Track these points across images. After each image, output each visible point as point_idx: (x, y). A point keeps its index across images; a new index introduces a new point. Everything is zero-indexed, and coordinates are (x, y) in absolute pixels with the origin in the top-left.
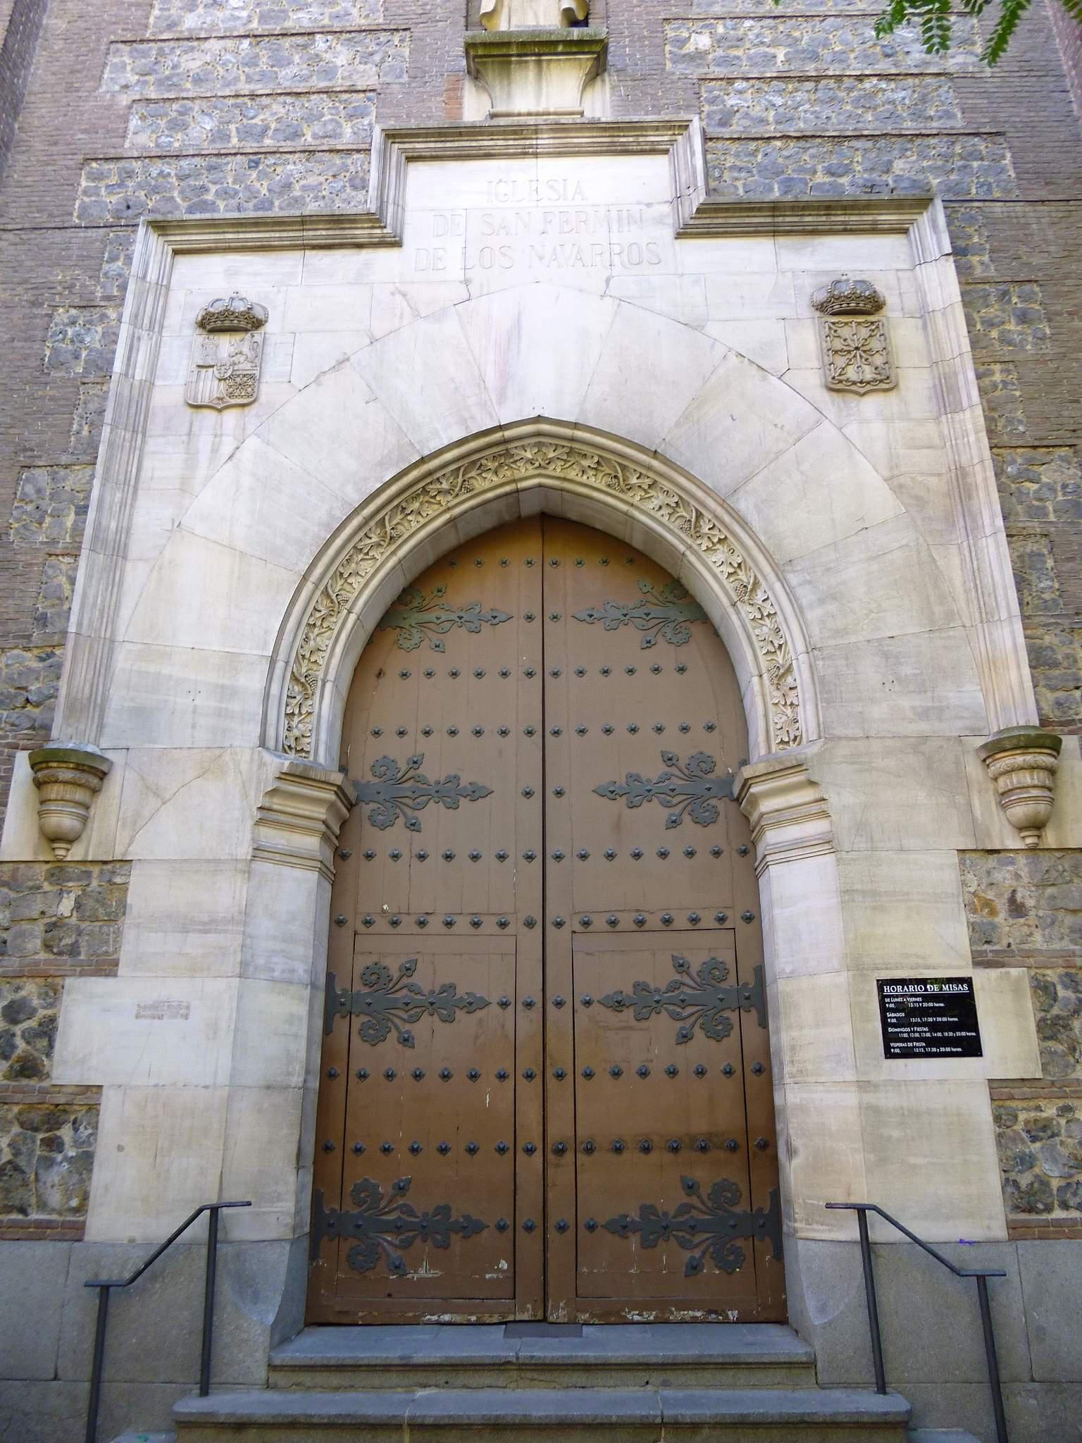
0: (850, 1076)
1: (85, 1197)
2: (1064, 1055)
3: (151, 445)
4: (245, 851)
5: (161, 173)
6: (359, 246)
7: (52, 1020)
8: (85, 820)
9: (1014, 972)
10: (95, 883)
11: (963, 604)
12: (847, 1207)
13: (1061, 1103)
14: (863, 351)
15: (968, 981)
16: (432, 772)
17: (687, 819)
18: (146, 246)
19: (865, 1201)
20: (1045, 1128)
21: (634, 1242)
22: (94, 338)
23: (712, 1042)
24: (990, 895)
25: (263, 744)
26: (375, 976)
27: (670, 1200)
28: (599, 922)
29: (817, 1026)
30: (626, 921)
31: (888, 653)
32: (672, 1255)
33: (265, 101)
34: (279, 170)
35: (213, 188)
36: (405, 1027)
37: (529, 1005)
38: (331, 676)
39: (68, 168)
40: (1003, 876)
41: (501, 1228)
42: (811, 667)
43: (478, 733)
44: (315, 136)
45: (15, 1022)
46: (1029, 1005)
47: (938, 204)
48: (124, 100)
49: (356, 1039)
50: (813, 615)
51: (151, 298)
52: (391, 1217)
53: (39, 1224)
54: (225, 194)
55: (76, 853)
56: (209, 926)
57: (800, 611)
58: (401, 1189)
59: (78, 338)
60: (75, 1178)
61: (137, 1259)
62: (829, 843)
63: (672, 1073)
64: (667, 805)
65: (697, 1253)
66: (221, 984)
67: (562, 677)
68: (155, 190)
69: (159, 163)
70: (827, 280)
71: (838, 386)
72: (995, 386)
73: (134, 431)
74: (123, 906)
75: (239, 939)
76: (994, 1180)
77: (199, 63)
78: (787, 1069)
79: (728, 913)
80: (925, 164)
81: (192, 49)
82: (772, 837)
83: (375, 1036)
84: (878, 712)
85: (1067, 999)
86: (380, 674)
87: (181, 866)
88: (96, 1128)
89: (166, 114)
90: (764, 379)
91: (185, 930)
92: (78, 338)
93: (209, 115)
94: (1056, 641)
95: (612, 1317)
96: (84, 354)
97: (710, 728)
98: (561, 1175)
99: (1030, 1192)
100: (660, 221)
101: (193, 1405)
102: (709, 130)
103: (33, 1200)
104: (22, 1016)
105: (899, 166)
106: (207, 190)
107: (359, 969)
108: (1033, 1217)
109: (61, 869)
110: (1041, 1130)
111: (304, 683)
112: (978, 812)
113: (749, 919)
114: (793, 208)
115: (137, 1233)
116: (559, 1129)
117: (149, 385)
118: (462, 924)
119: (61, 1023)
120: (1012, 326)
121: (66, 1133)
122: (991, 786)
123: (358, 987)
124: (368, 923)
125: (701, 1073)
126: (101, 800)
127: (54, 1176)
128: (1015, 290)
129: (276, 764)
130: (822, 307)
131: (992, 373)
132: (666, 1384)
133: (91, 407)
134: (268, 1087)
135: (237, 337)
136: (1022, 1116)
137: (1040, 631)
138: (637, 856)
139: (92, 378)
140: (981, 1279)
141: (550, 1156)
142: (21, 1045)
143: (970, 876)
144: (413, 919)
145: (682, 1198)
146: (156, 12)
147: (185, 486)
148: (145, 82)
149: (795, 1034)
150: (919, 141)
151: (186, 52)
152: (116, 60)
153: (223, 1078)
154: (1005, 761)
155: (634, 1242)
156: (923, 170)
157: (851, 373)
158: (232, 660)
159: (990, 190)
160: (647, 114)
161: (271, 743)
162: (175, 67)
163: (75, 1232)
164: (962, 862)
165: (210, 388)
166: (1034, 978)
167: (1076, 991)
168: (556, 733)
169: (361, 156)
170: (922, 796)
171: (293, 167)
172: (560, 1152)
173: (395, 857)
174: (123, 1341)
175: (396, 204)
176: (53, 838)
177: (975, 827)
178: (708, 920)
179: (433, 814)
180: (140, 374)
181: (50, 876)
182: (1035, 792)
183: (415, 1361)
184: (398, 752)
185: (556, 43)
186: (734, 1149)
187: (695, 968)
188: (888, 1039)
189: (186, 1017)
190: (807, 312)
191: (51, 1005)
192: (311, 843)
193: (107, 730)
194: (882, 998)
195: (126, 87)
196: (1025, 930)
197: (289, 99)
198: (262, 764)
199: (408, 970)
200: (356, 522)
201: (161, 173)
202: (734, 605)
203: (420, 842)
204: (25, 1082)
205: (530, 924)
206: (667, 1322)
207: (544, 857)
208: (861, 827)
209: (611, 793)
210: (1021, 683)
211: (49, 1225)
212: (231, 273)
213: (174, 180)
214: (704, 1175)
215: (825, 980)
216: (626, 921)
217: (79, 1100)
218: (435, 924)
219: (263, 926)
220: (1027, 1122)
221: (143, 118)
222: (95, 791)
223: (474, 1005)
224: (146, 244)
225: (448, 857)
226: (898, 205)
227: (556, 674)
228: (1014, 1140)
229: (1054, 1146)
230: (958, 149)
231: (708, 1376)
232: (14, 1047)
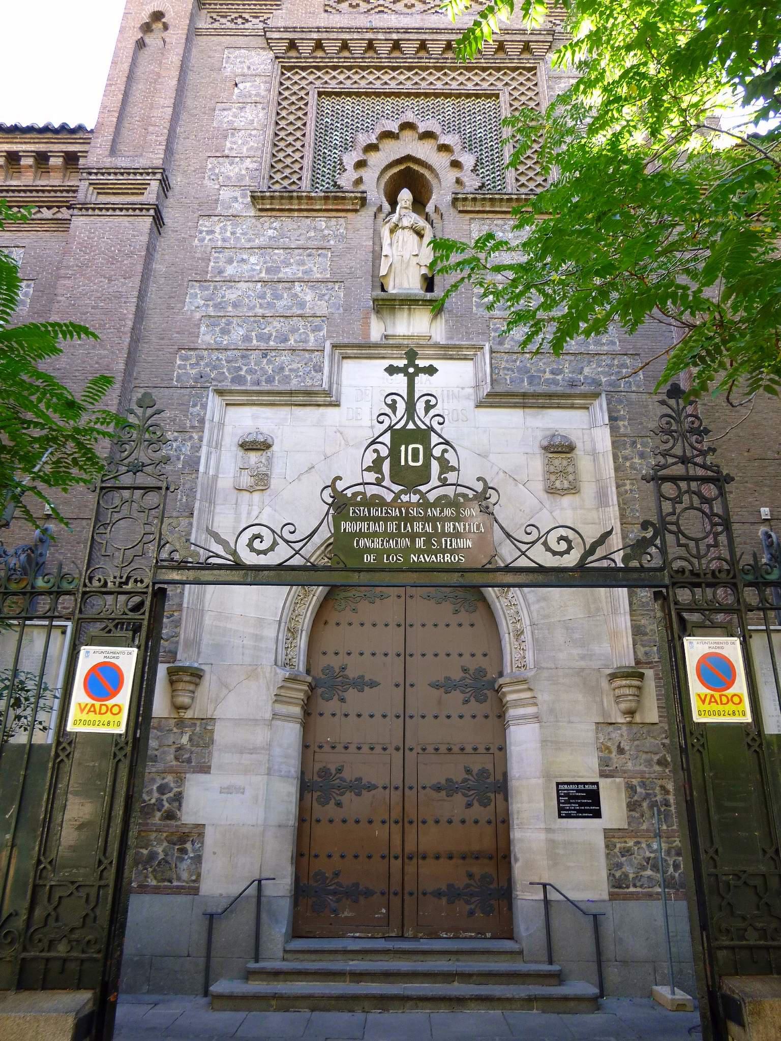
0: (543, 826)
1: (199, 875)
2: (638, 818)
3: (218, 509)
4: (268, 715)
5: (218, 358)
6: (319, 405)
7: (180, 793)
8: (193, 698)
9: (618, 780)
10: (198, 729)
11: (604, 604)
12: (538, 884)
13: (635, 840)
14: (563, 473)
15: (597, 784)
16: (352, 673)
17: (472, 699)
18: (214, 402)
19: (547, 882)
20: (628, 851)
21: (444, 900)
22: (187, 449)
23: (482, 808)
24: (609, 744)
25: (276, 664)
26: (324, 773)
27: (461, 882)
28: (430, 749)
29: (529, 802)
30: (443, 749)
31: (568, 626)
32: (461, 907)
33: (270, 320)
34: (277, 359)
35: (245, 368)
36: (338, 798)
37: (397, 788)
38: (305, 628)
39: (170, 353)
40: (616, 735)
41: (383, 894)
42: (532, 633)
43: (373, 654)
44: (295, 341)
45: (163, 794)
46: (624, 796)
47: (603, 396)
48: (198, 315)
49: (315, 804)
50: (534, 608)
51: (216, 431)
52: (332, 888)
53: (177, 887)
54: (250, 371)
55: (189, 714)
56: (253, 751)
57: (528, 606)
58: (337, 874)
59: (178, 449)
60: (194, 867)
61: (224, 903)
62: (537, 718)
63: (463, 822)
64: (463, 692)
65: (473, 906)
66: (259, 778)
67: (414, 627)
68: (215, 368)
69: (216, 353)
70: (548, 433)
71: (552, 491)
72: (626, 492)
73: (210, 502)
74: (212, 741)
75: (267, 757)
76: (604, 874)
77: (235, 296)
78: (515, 821)
79: (491, 746)
80: (600, 369)
81: (231, 287)
82: (512, 712)
83: (324, 802)
84: (562, 656)
85: (641, 793)
86: (326, 623)
87: (239, 722)
88: (202, 843)
89: (219, 325)
90: (516, 485)
91: (241, 753)
92: (178, 449)
93: (241, 326)
94: (647, 622)
95: (434, 935)
96: (182, 457)
97: (485, 655)
98: (411, 868)
99: (620, 879)
100: (468, 398)
101: (252, 965)
102: (494, 347)
103: (175, 876)
104: (166, 791)
105: (586, 371)
106: (241, 369)
107: (316, 769)
108: (621, 890)
109: (182, 722)
110: (627, 852)
111: (292, 632)
112: (605, 704)
113: (500, 749)
114: (533, 396)
115: (224, 893)
116: (410, 847)
117: (215, 477)
118: (365, 749)
119: (185, 795)
120: (636, 460)
121: (188, 846)
122: (612, 693)
123: (316, 778)
124: (321, 747)
125: (476, 822)
126: (200, 689)
127: (184, 865)
128: (639, 440)
129: (282, 674)
130: (545, 448)
131: (625, 485)
132: (458, 960)
133: (187, 486)
134: (279, 826)
135: (259, 453)
136: (618, 845)
137: (640, 617)
138: (449, 717)
139: (186, 471)
140: (595, 916)
141: (406, 860)
142: (166, 805)
143: (600, 735)
144: (342, 745)
145: (467, 881)
146: (212, 264)
148: (208, 305)
149: (519, 805)
150: (597, 357)
151: (228, 289)
152: (192, 291)
153: (260, 822)
154: (619, 682)
155: (444, 900)
156: (598, 373)
157: (558, 484)
158: (260, 622)
159: (630, 387)
160: (462, 339)
161: (279, 663)
162: (223, 297)
163: (195, 891)
164: (597, 728)
165: (246, 480)
166: (627, 783)
167: (646, 789)
168: (411, 655)
169: (319, 353)
170: (580, 697)
171: (285, 358)
172: (410, 858)
173: (334, 715)
174: (220, 939)
175: (338, 384)
176: (178, 708)
177: (604, 713)
178: (482, 749)
179: (351, 694)
180: (212, 472)
181: (177, 725)
182: (630, 698)
183: (349, 949)
184: (335, 663)
185: (419, 300)
186: (491, 858)
187: (475, 771)
188: (560, 809)
189: (243, 793)
190: (538, 451)
191: (179, 787)
192: (297, 710)
193: (202, 655)
194: (558, 790)
195: (198, 307)
196: (624, 761)
197: (282, 319)
198: (276, 674)
199: (339, 770)
200: (318, 553)
201: (218, 358)
202: (498, 598)
203: (345, 708)
204: (169, 822)
205: (397, 749)
206: (458, 938)
207: (404, 716)
208: (552, 711)
209: (436, 686)
210: (628, 647)
211: (182, 887)
212: (255, 417)
213: (224, 362)
214: (476, 870)
215: (534, 781)
216: (443, 749)
217: (195, 830)
218: (353, 748)
219: (277, 751)
220: (620, 848)
221: (207, 326)
222: (197, 685)
223: (371, 787)
224: (213, 402)
225: (359, 716)
226: (584, 396)
227: (411, 626)
228: (614, 856)
229: (631, 860)
230: (616, 362)
231: (476, 957)
232: (163, 806)
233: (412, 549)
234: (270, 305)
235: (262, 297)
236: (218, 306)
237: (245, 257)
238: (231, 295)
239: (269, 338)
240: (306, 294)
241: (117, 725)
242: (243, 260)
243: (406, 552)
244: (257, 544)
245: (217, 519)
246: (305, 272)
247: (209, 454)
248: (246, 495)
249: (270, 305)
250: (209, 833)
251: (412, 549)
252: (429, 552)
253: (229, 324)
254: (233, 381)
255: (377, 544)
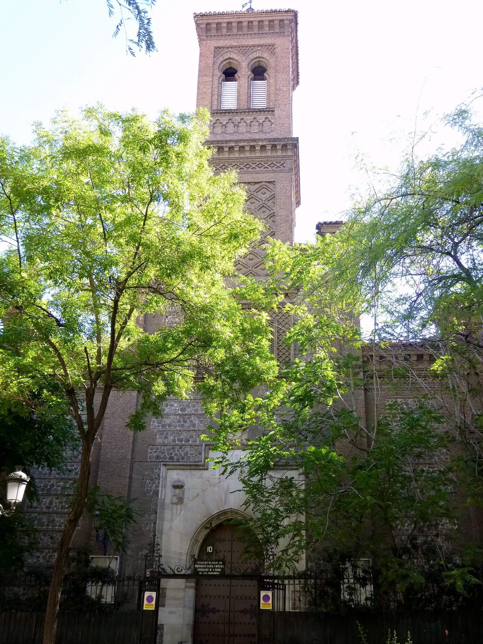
1: (162, 641)
4: (184, 587)
18: (163, 469)
26: (203, 606)
28: (239, 598)
30: (243, 597)
48: (155, 431)
56: (179, 599)
59: (151, 487)
68: (163, 453)
74: (165, 596)
111: (196, 541)
117: (164, 499)
118: (217, 597)
147: (172, 520)
158: (181, 554)
165: (175, 500)
199: (208, 605)
205: (228, 597)
216: (243, 597)
219: (187, 599)
223: (219, 611)
233: (209, 571)
234: (182, 426)
235: (179, 422)
236: (163, 426)
237: (172, 403)
238: (168, 421)
239: (182, 441)
240: (196, 420)
241: (153, 608)
242: (172, 405)
243: (208, 572)
244: (179, 570)
245: (165, 515)
246: (195, 410)
247: (162, 490)
248: (175, 505)
249: (182, 426)
250: (165, 627)
251: (209, 571)
252: (212, 571)
253: (167, 434)
254: (170, 458)
255: (202, 570)
